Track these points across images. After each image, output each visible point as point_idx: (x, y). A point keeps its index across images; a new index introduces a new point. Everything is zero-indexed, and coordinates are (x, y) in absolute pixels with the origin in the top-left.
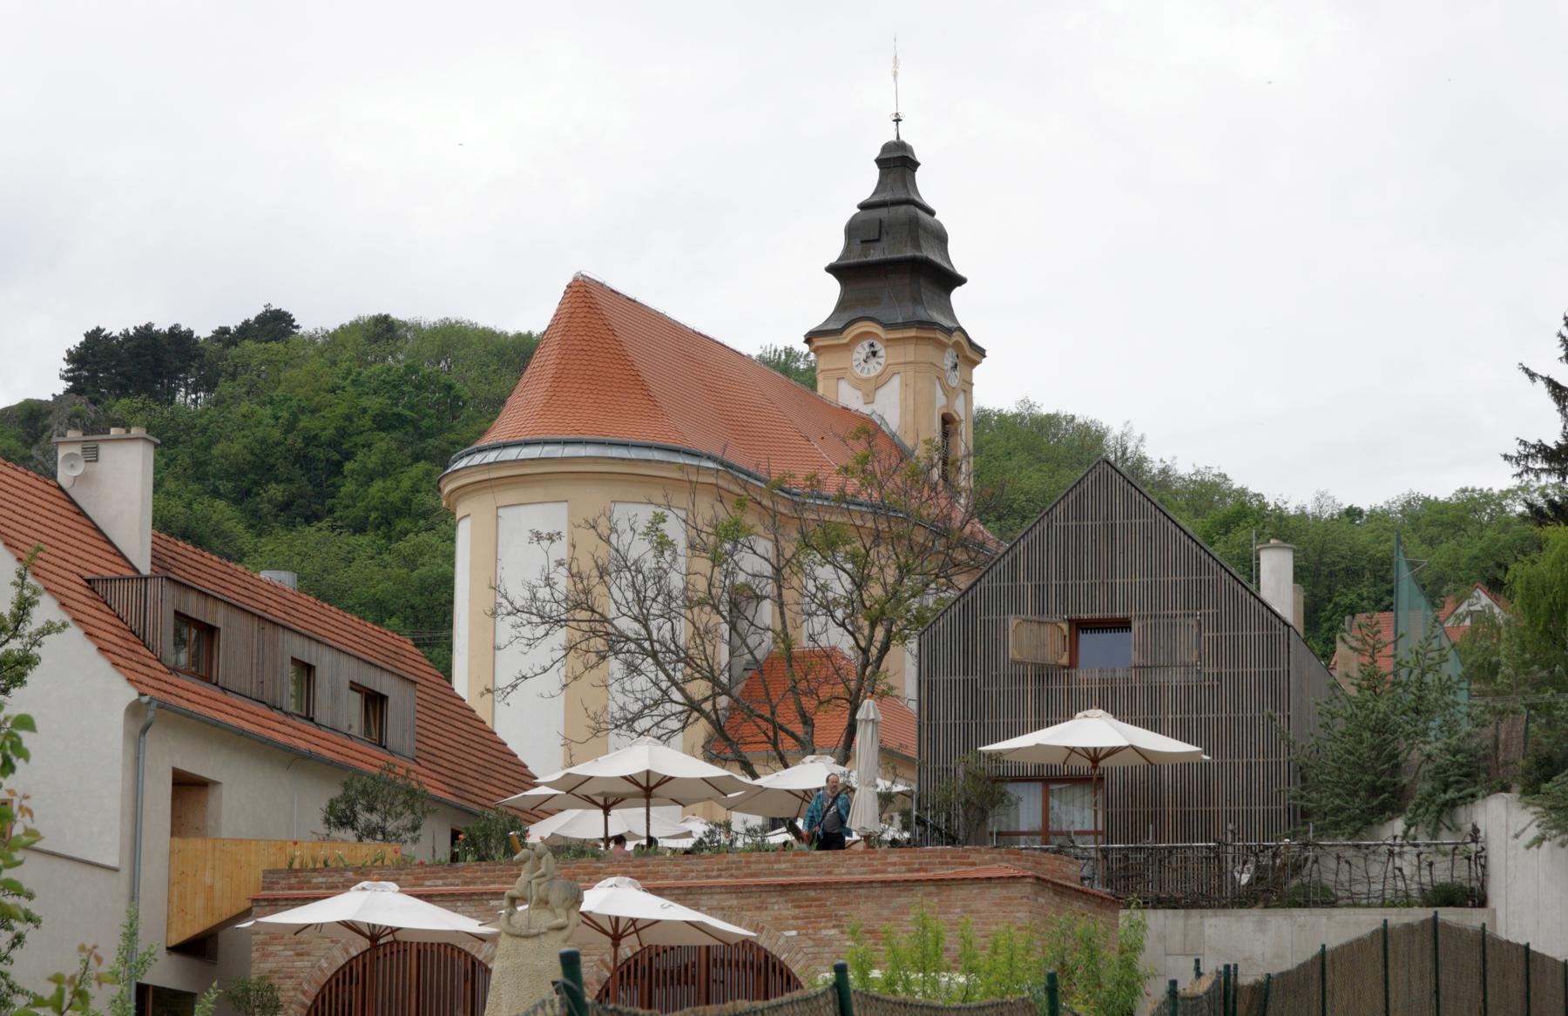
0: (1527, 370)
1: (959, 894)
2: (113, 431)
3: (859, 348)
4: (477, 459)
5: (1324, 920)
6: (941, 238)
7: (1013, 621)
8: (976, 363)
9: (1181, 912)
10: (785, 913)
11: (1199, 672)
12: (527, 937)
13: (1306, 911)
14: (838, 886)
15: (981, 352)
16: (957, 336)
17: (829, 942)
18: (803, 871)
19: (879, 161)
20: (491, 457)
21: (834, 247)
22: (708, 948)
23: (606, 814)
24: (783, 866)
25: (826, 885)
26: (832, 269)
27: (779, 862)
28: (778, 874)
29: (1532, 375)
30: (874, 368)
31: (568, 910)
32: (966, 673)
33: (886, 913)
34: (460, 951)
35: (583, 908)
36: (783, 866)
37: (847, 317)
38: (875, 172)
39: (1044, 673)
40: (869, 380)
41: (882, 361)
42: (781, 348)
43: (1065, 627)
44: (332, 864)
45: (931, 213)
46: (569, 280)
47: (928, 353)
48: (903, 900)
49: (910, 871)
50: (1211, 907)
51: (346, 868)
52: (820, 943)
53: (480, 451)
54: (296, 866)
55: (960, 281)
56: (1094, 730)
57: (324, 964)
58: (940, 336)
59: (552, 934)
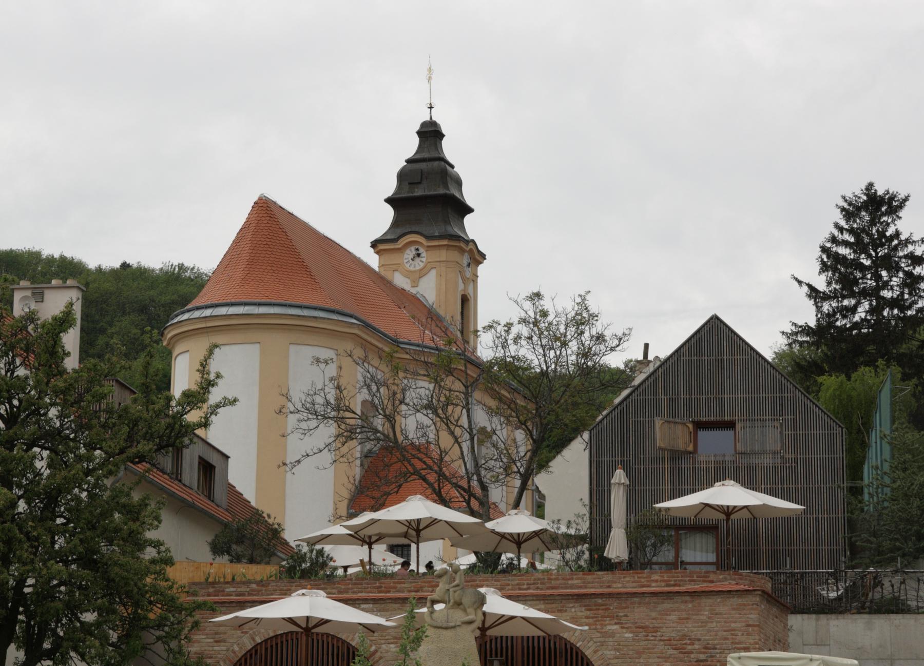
0: (796, 279)
1: (706, 602)
2: (54, 282)
3: (408, 251)
4: (186, 316)
5: (912, 622)
6: (458, 183)
7: (658, 422)
8: (481, 263)
9: (814, 616)
10: (580, 614)
11: (782, 457)
12: (446, 628)
13: (900, 616)
14: (618, 596)
15: (483, 256)
16: (471, 246)
17: (612, 634)
18: (590, 585)
19: (419, 133)
20: (197, 314)
21: (390, 187)
22: (539, 637)
23: (370, 548)
24: (575, 582)
25: (610, 595)
26: (389, 201)
27: (572, 579)
28: (572, 587)
29: (800, 283)
30: (419, 264)
31: (476, 610)
32: (622, 455)
33: (654, 614)
34: (339, 639)
35: (485, 608)
36: (575, 582)
37: (399, 231)
38: (416, 140)
39: (676, 456)
40: (415, 271)
41: (424, 260)
42: (176, 263)
43: (691, 426)
44: (237, 579)
45: (452, 167)
46: (256, 199)
47: (454, 255)
48: (667, 605)
49: (667, 586)
50: (835, 613)
51: (249, 582)
52: (606, 635)
53: (189, 311)
54: (210, 580)
55: (470, 210)
56: (729, 494)
57: (236, 648)
58: (462, 245)
59: (464, 626)
